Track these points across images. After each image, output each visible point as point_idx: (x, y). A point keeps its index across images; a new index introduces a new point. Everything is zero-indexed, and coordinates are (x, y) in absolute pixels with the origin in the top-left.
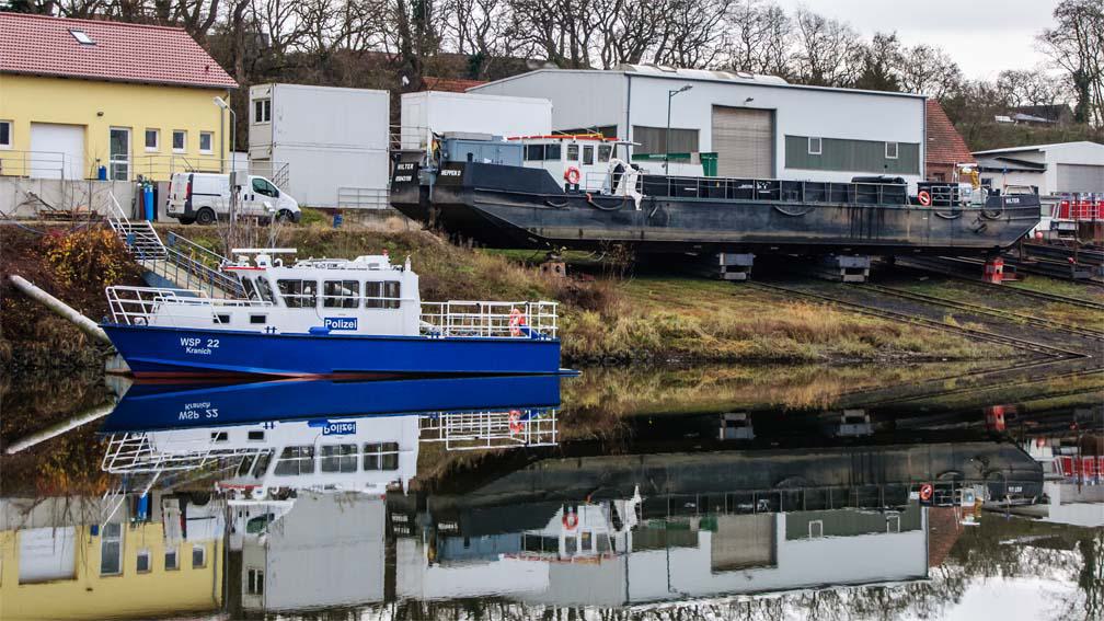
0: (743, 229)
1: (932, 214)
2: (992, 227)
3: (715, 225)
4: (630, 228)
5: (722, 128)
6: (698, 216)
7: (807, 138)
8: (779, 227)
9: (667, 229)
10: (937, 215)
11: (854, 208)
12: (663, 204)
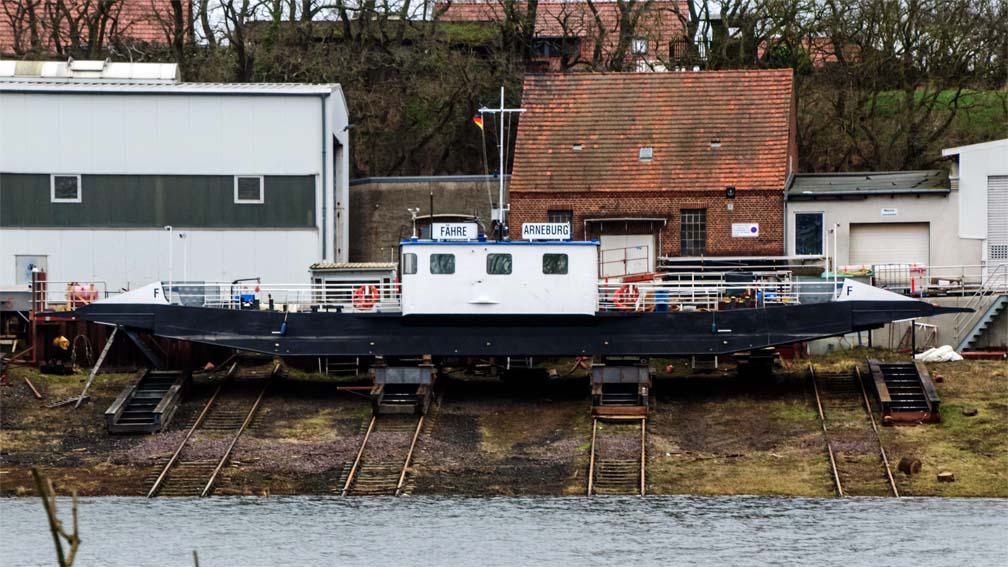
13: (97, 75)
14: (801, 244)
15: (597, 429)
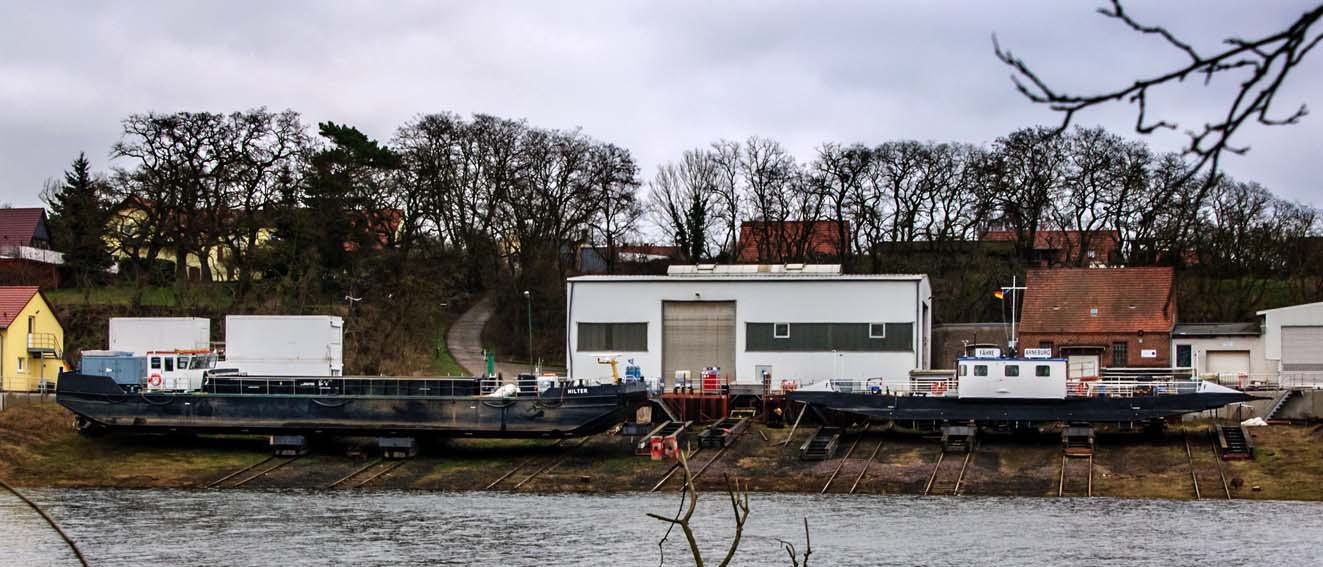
5: (677, 320)
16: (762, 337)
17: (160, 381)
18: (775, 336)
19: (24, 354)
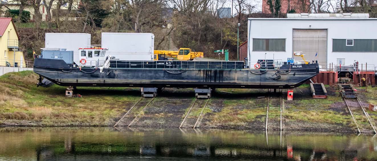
0: (151, 78)
1: (250, 72)
2: (283, 77)
3: (138, 77)
4: (99, 79)
5: (300, 37)
6: (130, 74)
7: (346, 39)
8: (169, 78)
9: (116, 79)
10: (252, 73)
11: (207, 71)
12: (113, 70)
13: (350, 16)
14: (236, 50)
15: (364, 110)
16: (340, 46)
17: (86, 62)
18: (347, 45)
19: (7, 50)
